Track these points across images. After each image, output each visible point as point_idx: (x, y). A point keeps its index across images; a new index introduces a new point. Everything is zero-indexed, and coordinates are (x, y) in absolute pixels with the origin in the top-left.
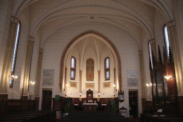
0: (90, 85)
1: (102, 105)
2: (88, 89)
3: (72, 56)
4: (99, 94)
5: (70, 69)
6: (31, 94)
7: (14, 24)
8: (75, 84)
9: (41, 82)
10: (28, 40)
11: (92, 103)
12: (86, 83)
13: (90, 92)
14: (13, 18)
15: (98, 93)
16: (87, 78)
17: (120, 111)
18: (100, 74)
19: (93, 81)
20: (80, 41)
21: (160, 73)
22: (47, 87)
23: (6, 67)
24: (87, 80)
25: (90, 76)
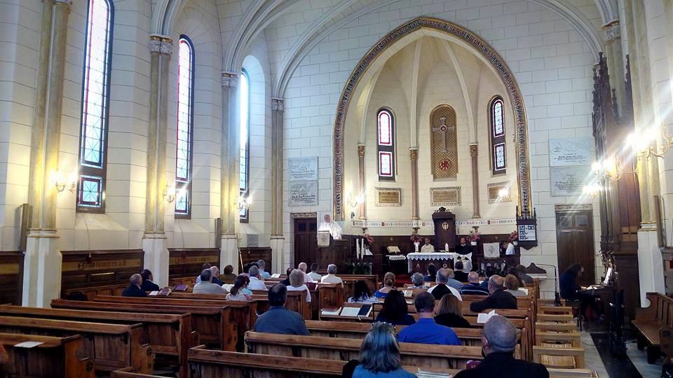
0: (446, 193)
3: (377, 109)
4: (477, 222)
5: (375, 149)
6: (256, 230)
7: (160, 57)
8: (394, 193)
9: (287, 196)
10: (223, 86)
13: (442, 218)
14: (156, 41)
16: (433, 173)
20: (400, 54)
22: (304, 209)
23: (156, 170)
25: (445, 164)
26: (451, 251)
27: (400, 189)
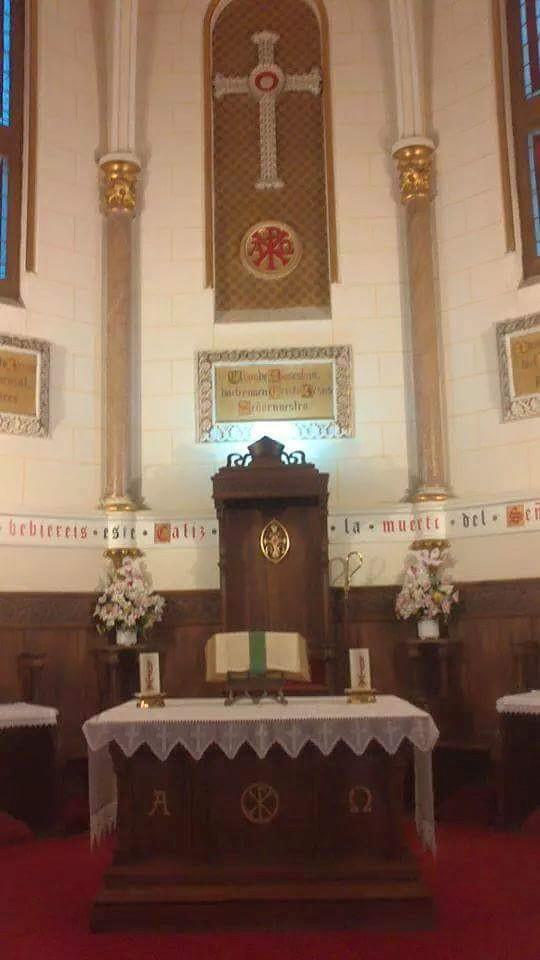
1: (509, 703)
2: (236, 441)
8: (14, 363)
11: (285, 687)
12: (207, 357)
18: (430, 192)
21: (423, 512)
26: (382, 687)
27: (43, 347)
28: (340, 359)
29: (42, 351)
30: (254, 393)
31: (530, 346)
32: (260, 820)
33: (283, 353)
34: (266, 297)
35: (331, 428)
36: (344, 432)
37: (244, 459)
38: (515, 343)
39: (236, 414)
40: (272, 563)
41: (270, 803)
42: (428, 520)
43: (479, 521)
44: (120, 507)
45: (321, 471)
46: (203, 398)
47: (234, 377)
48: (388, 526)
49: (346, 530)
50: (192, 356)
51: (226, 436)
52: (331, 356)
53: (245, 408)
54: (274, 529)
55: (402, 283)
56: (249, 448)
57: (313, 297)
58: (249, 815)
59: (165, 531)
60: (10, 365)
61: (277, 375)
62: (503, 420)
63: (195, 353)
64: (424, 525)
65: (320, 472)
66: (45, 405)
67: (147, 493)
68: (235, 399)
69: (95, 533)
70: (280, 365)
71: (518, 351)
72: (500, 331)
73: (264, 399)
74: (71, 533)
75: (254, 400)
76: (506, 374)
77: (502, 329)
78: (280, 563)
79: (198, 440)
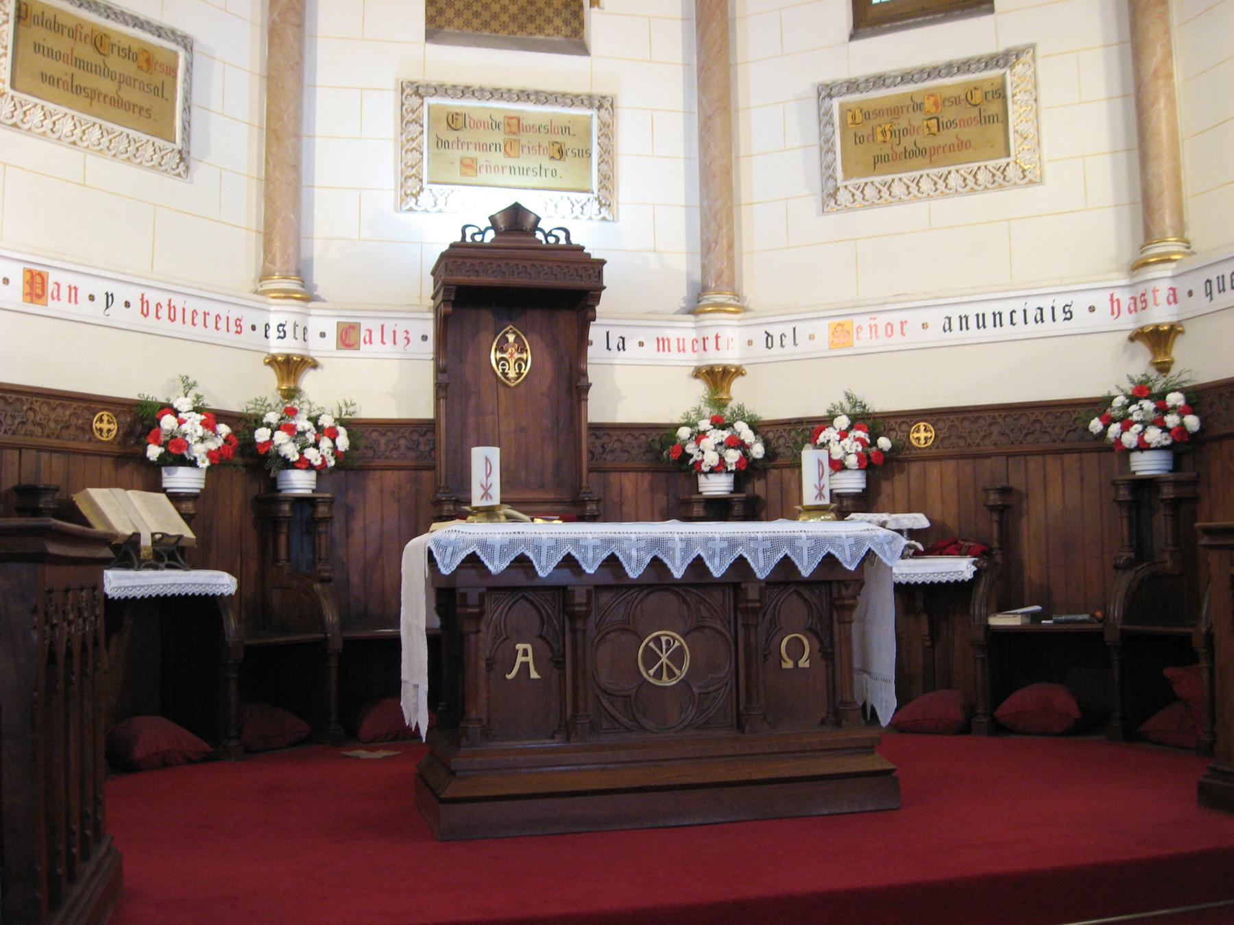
15: (694, 309)
17: (928, 638)
19: (576, 43)
24: (435, 31)
28: (603, 111)
29: (185, 47)
30: (485, 147)
31: (867, 116)
32: (666, 682)
33: (524, 95)
34: (495, 16)
35: (589, 205)
36: (604, 212)
37: (483, 233)
38: (844, 110)
39: (456, 176)
40: (506, 386)
41: (677, 657)
42: (717, 337)
43: (788, 341)
44: (287, 295)
45: (596, 255)
46: (408, 145)
47: (454, 121)
48: (662, 344)
49: (608, 348)
50: (391, 84)
51: (441, 205)
52: (591, 106)
53: (467, 166)
54: (511, 338)
55: (685, 19)
56: (492, 219)
57: (543, 23)
58: (648, 675)
59: (353, 334)
60: (142, 58)
61: (515, 125)
62: (824, 209)
63: (397, 80)
64: (711, 344)
65: (592, 257)
66: (186, 129)
67: (321, 279)
68: (456, 154)
69: (254, 328)
70: (522, 111)
71: (850, 121)
72: (823, 94)
73: (497, 158)
74: (223, 324)
75: (482, 157)
76: (831, 150)
77: (827, 91)
78: (517, 386)
79: (398, 209)
